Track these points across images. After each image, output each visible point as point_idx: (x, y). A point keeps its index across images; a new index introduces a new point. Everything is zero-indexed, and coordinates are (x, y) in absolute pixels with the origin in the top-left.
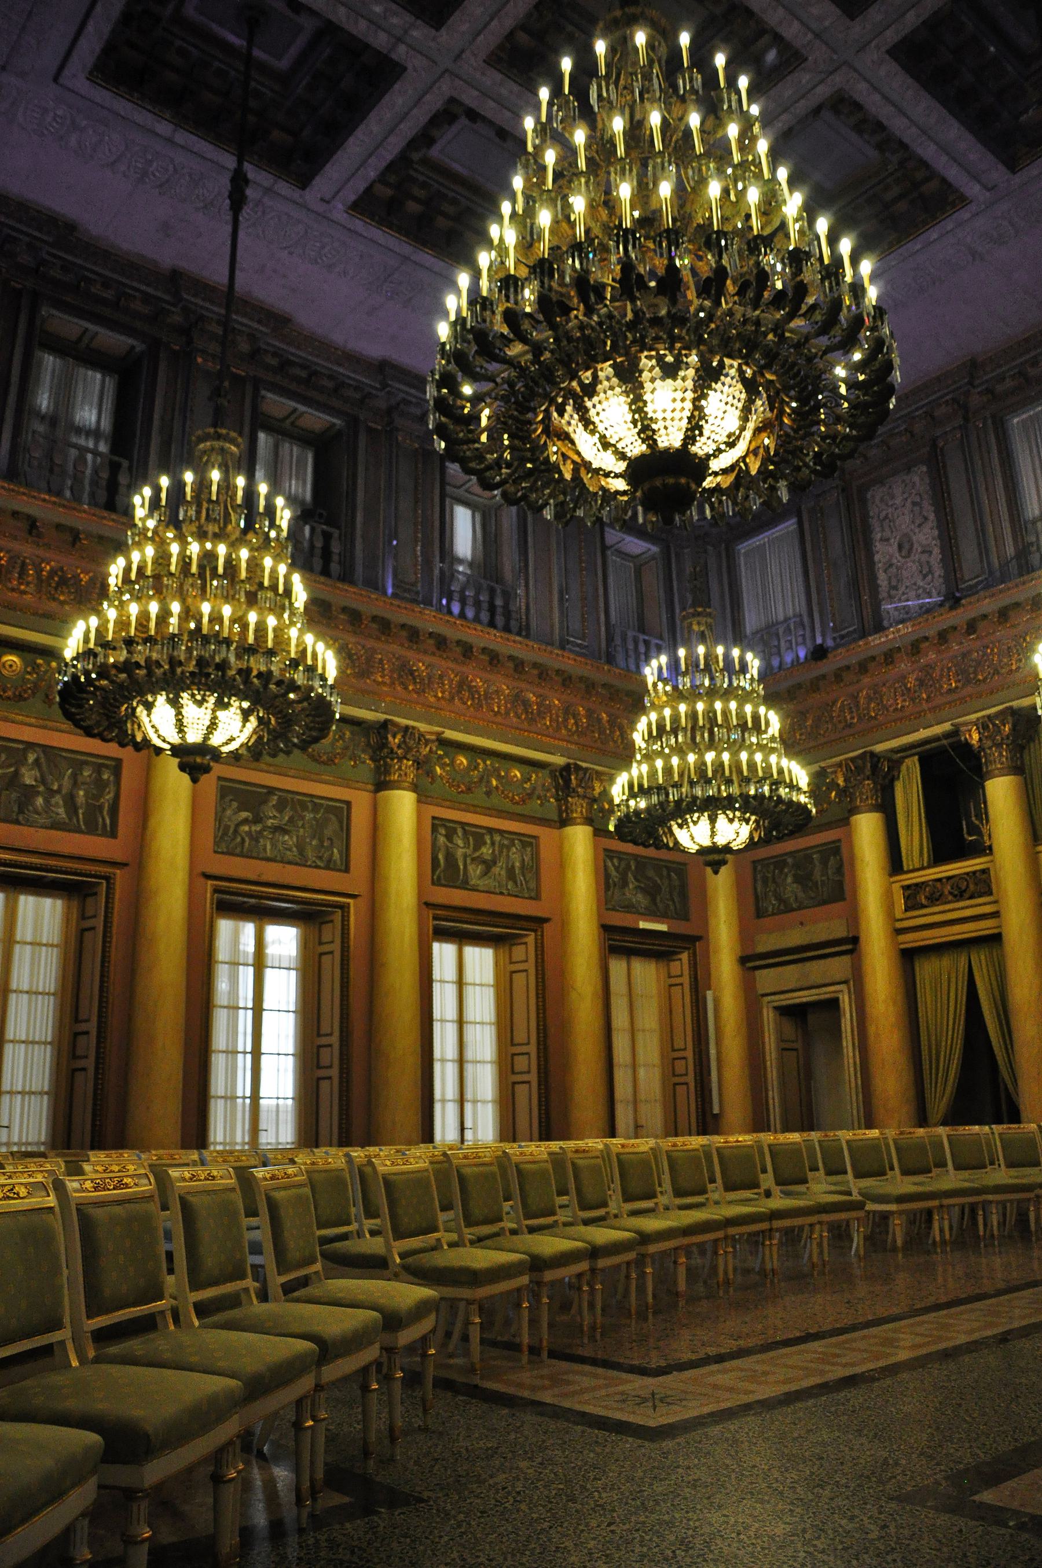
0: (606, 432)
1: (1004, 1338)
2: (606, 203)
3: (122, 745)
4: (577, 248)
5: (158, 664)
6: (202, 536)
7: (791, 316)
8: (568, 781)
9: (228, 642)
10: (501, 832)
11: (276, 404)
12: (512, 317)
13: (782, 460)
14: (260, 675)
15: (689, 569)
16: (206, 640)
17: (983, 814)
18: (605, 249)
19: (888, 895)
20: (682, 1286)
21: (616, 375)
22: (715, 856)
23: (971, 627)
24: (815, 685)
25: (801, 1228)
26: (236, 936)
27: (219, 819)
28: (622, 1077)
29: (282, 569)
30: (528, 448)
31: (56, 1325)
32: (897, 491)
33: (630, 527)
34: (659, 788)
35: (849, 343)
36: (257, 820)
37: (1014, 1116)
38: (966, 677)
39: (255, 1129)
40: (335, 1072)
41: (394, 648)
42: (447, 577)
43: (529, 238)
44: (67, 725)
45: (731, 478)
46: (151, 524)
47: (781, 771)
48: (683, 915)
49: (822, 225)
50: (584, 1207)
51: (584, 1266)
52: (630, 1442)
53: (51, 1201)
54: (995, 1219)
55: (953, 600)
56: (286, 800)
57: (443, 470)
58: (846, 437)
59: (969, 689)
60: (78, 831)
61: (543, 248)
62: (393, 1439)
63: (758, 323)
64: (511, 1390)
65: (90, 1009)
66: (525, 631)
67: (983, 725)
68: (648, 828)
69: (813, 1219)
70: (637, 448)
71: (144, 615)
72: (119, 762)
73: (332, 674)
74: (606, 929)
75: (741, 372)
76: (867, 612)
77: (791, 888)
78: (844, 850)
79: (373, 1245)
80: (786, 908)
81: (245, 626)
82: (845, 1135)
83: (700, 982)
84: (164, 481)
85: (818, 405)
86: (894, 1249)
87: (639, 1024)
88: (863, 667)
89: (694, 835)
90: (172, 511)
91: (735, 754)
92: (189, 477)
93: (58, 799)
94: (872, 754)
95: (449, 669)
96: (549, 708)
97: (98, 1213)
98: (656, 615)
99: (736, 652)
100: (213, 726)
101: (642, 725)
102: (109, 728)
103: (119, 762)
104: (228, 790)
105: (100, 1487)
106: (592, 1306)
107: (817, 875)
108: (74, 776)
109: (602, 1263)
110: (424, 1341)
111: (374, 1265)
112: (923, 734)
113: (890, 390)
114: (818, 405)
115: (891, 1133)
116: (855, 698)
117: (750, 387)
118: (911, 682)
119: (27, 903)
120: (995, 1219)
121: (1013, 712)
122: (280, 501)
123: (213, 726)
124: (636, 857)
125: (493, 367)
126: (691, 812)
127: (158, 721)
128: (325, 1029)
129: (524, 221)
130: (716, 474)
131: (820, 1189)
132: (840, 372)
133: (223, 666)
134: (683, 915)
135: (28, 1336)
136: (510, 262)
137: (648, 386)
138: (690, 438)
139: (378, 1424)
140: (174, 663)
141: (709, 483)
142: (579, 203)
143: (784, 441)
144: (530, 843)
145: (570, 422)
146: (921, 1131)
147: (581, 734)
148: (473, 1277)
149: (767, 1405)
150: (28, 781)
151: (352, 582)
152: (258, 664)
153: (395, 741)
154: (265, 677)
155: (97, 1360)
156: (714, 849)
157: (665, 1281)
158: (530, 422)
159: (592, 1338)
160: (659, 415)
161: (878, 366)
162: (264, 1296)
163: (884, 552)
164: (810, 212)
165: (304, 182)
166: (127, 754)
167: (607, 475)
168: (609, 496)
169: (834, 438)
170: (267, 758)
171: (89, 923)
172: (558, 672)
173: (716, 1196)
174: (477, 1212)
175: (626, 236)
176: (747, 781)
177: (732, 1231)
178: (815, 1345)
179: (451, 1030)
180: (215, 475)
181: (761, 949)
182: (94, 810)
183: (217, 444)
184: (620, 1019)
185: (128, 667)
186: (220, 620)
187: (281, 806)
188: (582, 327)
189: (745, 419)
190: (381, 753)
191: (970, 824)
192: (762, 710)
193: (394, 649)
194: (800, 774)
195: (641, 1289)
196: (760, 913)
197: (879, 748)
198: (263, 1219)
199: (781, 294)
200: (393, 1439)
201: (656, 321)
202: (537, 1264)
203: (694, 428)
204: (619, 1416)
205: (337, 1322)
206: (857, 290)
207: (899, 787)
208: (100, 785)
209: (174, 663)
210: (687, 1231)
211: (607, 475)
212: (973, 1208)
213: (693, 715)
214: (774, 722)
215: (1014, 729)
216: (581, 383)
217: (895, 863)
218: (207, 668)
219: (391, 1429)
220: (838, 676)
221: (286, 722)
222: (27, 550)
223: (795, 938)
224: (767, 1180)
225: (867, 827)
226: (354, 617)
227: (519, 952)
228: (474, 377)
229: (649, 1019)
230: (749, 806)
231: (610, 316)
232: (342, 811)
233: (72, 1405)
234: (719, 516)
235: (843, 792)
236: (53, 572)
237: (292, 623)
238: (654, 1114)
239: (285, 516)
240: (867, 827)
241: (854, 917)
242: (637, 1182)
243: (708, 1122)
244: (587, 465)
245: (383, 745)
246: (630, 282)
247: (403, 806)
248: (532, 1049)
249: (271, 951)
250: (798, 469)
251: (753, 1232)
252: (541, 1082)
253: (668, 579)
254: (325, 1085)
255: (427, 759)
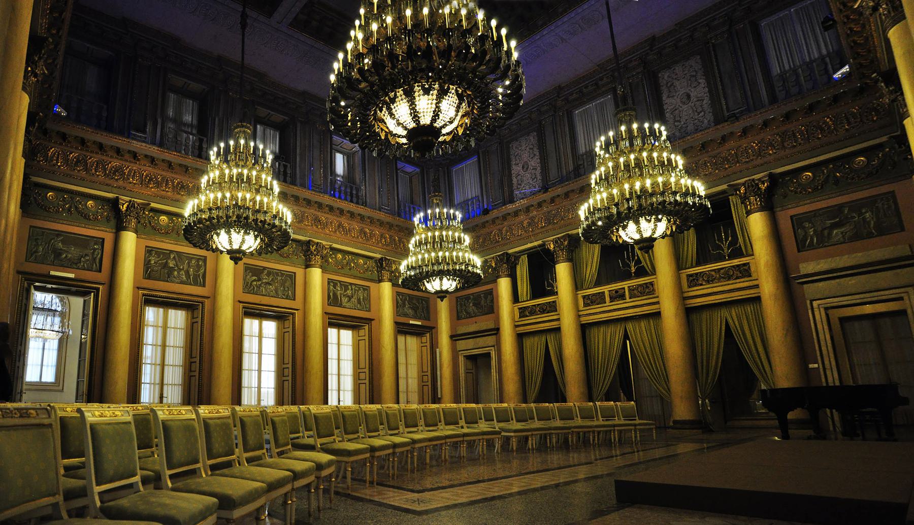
0: (398, 118)
1: (557, 485)
2: (399, 18)
3: (208, 250)
4: (388, 39)
5: (222, 217)
6: (237, 166)
7: (480, 65)
8: (382, 264)
9: (248, 208)
10: (355, 285)
11: (262, 112)
12: (361, 71)
13: (472, 130)
14: (261, 221)
15: (432, 178)
16: (240, 208)
17: (554, 279)
18: (401, 39)
19: (513, 312)
20: (428, 461)
21: (404, 94)
22: (442, 294)
23: (553, 200)
24: (484, 225)
25: (474, 441)
26: (251, 325)
27: (244, 279)
28: (402, 383)
29: (269, 179)
30: (367, 126)
31: (197, 462)
32: (523, 143)
33: (409, 161)
34: (420, 266)
35: (504, 77)
36: (259, 280)
37: (564, 400)
38: (549, 221)
39: (259, 400)
40: (290, 378)
41: (312, 211)
42: (333, 182)
43: (368, 37)
44: (186, 243)
45: (451, 137)
46: (217, 162)
47: (469, 260)
48: (427, 318)
49: (494, 23)
50: (390, 429)
51: (391, 451)
52: (410, 516)
53: (194, 416)
54: (554, 440)
55: (545, 189)
56: (271, 272)
57: (331, 138)
58: (500, 118)
59: (550, 227)
60: (190, 284)
61: (374, 40)
62: (319, 511)
63: (465, 69)
64: (363, 496)
65: (196, 353)
66: (365, 204)
67: (555, 242)
68: (415, 282)
69: (481, 437)
70: (412, 125)
71: (216, 198)
72: (206, 257)
73: (289, 221)
74: (396, 323)
75: (457, 91)
76: (507, 194)
77: (472, 308)
78: (494, 293)
79: (311, 441)
80: (469, 316)
81: (255, 203)
82: (494, 406)
83: (434, 345)
84: (222, 145)
85: (489, 104)
86: (512, 450)
87: (409, 362)
88: (504, 218)
89: (433, 285)
90: (225, 156)
91: (451, 253)
92: (232, 143)
93: (182, 272)
94: (507, 254)
95: (334, 219)
96: (374, 235)
97: (210, 422)
98: (418, 199)
99: (452, 211)
100: (243, 242)
101: (413, 241)
102: (203, 243)
103: (206, 257)
104: (248, 269)
105: (218, 518)
106: (393, 467)
107: (483, 302)
108: (189, 263)
109: (398, 450)
110: (331, 475)
111: (311, 448)
112: (530, 245)
113: (521, 97)
114: (489, 104)
115: (512, 405)
116: (500, 230)
117: (460, 97)
118: (525, 224)
119: (172, 312)
120: (554, 440)
121: (569, 235)
122: (268, 152)
123: (243, 242)
124: (409, 295)
125: (355, 93)
126: (432, 276)
127: (222, 240)
128: (286, 361)
129: (365, 28)
130: (444, 135)
131: (483, 426)
132: (500, 90)
133: (247, 218)
134: (427, 318)
135: (188, 465)
136: (360, 47)
137: (417, 98)
138: (434, 120)
139: (314, 504)
140: (228, 217)
141: (441, 139)
142: (389, 20)
143: (474, 121)
144: (366, 289)
145: (384, 114)
146: (524, 405)
147: (387, 245)
148: (349, 453)
149: (462, 505)
150: (171, 265)
151: (295, 185)
152: (261, 217)
153: (313, 248)
154: (264, 222)
155: (212, 475)
156: (441, 291)
157: (421, 459)
158: (368, 115)
159: (393, 478)
160: (421, 111)
161: (516, 87)
162: (271, 457)
163: (516, 169)
164: (488, 19)
165: (270, 15)
166: (208, 254)
167: (399, 137)
168: (400, 145)
169: (495, 118)
170: (263, 255)
171: (195, 320)
172: (378, 220)
173: (441, 427)
174: (349, 429)
175: (409, 33)
176: (456, 263)
177: (448, 440)
178: (482, 484)
179: (335, 362)
180: (242, 142)
181: (459, 332)
182: (196, 277)
183: (242, 129)
184: (402, 359)
185: (210, 219)
186: (245, 199)
187: (269, 274)
188: (390, 74)
189: (457, 111)
190: (307, 253)
191: (548, 283)
192: (462, 235)
193: (312, 211)
194: (477, 261)
195: (412, 463)
196: (459, 318)
197: (510, 251)
198: (270, 427)
199: (475, 55)
200: (319, 511)
201: (422, 70)
202: (373, 449)
203: (436, 116)
204: (405, 506)
205: (300, 466)
206: (509, 53)
207: (518, 268)
208: (198, 266)
209: (228, 217)
210: (430, 440)
211: (399, 137)
212: (545, 435)
213: (434, 237)
214: (467, 239)
215: (569, 243)
216: (389, 98)
217: (515, 298)
218: (241, 219)
219: (319, 507)
220: (493, 221)
221: (272, 240)
222: (169, 175)
223: (472, 328)
224: (462, 422)
225: (504, 285)
226: (296, 199)
227: (362, 332)
228: (346, 98)
229: (413, 359)
230: (454, 274)
231: (402, 69)
232: (292, 277)
233: (206, 488)
234: (445, 153)
235: (494, 269)
236: (178, 183)
237: (273, 200)
238: (414, 397)
239: (270, 158)
240: (504, 285)
241: (497, 320)
242: (410, 420)
243: (436, 399)
244: (391, 132)
245: (309, 249)
246: (411, 53)
247: (316, 275)
248: (367, 370)
249: (265, 332)
250: (479, 132)
251: (455, 442)
252: (369, 381)
253: (423, 183)
254: (286, 383)
255: (326, 256)
